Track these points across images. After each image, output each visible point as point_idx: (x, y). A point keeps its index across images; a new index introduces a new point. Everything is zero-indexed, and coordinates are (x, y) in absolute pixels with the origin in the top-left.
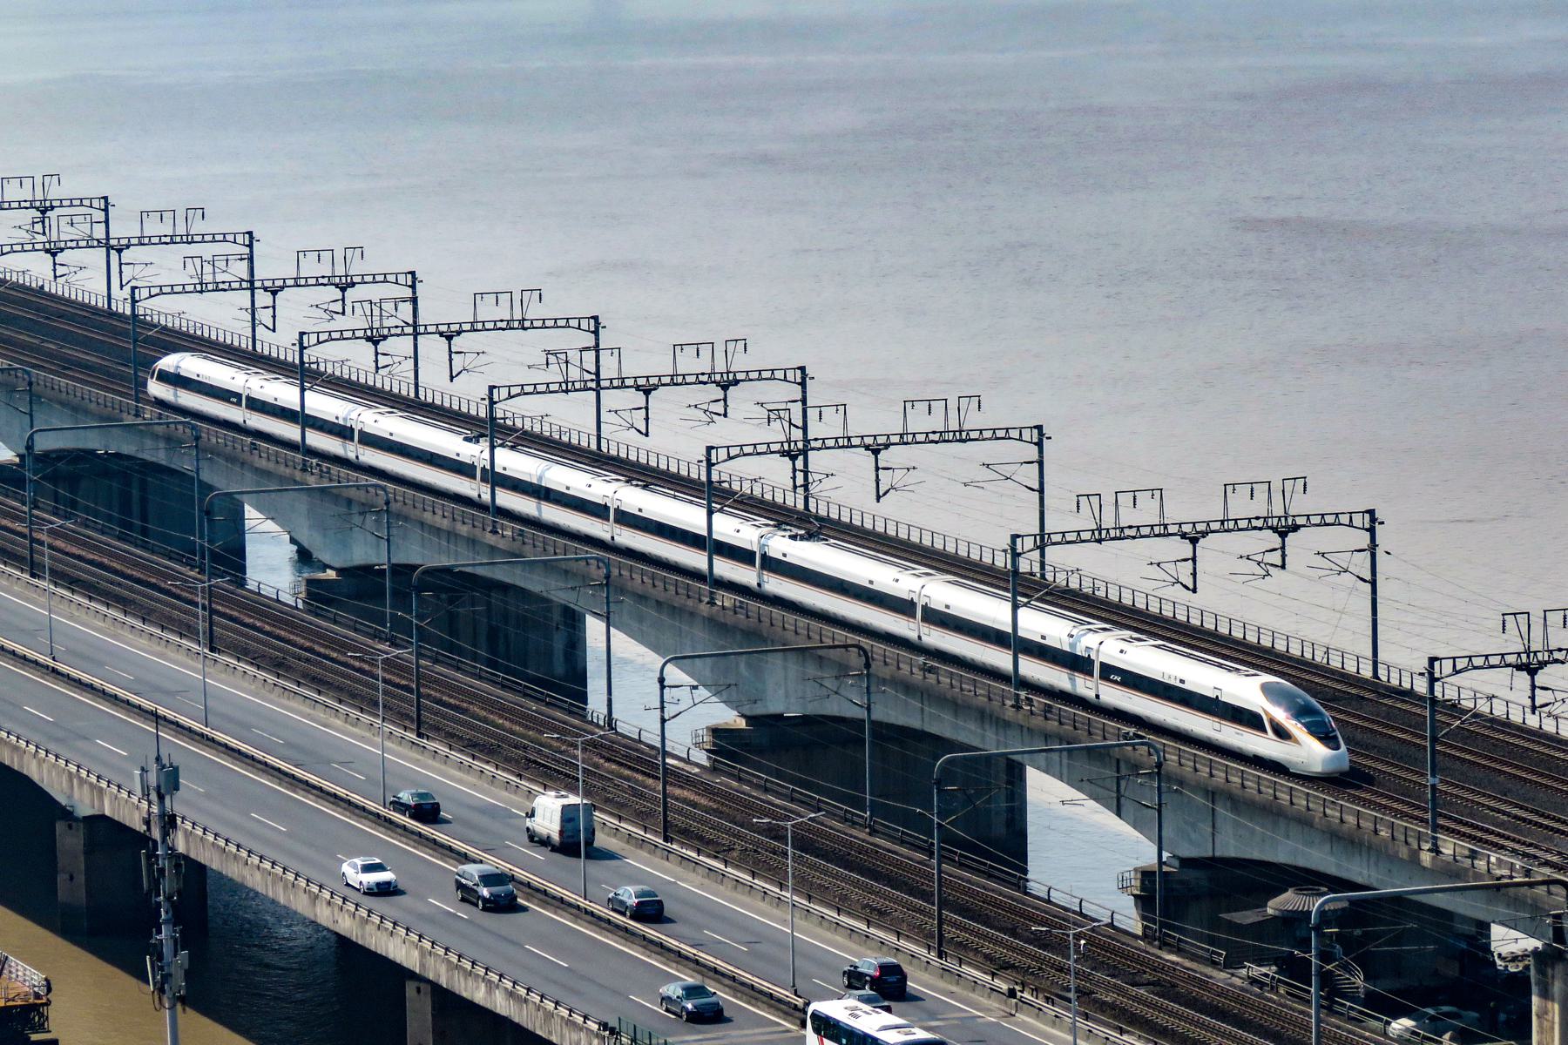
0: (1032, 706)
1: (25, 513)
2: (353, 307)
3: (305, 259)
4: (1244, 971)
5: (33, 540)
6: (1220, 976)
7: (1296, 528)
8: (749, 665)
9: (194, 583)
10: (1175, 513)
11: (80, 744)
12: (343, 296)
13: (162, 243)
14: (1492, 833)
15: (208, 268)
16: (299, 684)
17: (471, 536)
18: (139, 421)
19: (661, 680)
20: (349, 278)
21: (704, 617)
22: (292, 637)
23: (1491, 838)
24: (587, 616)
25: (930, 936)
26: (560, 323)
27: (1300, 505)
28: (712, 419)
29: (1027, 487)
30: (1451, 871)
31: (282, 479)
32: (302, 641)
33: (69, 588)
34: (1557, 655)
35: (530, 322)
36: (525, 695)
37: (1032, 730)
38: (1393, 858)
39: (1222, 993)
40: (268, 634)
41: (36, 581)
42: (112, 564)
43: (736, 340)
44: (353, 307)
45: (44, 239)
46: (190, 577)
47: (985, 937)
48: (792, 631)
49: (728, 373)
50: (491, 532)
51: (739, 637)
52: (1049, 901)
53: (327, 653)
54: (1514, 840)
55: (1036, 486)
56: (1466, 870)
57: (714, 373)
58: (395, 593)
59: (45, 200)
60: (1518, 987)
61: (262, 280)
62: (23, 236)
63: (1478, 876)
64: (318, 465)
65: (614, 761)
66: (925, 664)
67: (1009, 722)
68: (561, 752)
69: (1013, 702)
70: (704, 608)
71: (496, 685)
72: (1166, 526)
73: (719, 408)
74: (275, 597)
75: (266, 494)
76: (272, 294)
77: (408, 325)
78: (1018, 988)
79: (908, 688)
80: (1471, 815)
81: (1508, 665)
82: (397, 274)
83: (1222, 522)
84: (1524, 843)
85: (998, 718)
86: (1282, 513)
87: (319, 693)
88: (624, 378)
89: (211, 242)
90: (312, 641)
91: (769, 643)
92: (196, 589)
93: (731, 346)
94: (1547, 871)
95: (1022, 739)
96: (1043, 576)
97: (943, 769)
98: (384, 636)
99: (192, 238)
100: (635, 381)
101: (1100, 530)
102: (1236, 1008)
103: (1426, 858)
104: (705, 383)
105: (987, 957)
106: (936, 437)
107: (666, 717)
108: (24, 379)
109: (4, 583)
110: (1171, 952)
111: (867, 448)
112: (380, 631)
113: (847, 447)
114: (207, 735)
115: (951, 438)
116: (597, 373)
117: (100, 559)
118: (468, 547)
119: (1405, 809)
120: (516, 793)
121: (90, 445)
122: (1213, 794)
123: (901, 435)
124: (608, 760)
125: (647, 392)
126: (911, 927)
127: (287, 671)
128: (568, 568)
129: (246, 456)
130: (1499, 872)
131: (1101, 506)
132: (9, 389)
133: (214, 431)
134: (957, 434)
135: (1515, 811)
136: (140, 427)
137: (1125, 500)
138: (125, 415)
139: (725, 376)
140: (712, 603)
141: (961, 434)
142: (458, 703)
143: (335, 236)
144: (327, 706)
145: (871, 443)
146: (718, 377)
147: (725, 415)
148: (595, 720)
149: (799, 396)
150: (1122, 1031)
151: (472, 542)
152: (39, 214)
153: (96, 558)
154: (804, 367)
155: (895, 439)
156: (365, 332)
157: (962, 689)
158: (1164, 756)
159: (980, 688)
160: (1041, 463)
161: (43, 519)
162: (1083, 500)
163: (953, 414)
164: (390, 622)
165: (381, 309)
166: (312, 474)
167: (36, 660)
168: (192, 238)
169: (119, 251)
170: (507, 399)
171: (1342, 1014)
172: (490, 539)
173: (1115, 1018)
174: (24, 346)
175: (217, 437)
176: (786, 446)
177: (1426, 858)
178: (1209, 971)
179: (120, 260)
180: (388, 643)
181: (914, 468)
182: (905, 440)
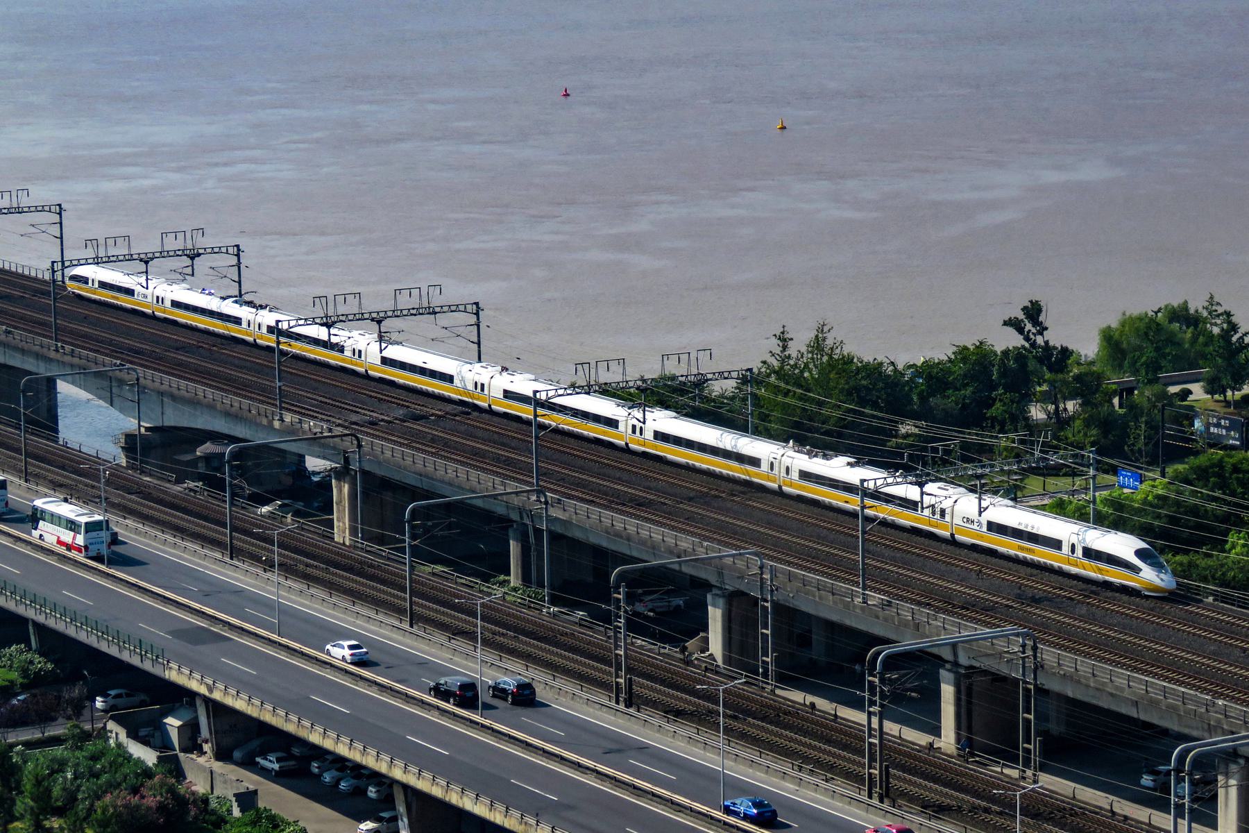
4: (186, 485)
6: (178, 488)
7: (199, 255)
9: (717, 685)
14: (310, 410)
23: (312, 413)
25: (21, 471)
27: (202, 242)
30: (290, 430)
34: (341, 318)
38: (259, 425)
39: (175, 496)
47: (49, 471)
52: (80, 451)
54: (321, 414)
55: (59, 236)
56: (298, 430)
60: (325, 487)
63: (304, 432)
72: (132, 255)
74: (1148, 821)
78: (69, 497)
80: (298, 402)
81: (316, 324)
83: (161, 253)
84: (327, 415)
86: (427, 305)
94: (340, 429)
96: (63, 282)
97: (25, 384)
101: (97, 258)
102: (184, 504)
103: (277, 424)
105: (51, 481)
106: (414, 312)
110: (146, 476)
119: (264, 399)
120: (659, 731)
122: (162, 394)
126: (10, 467)
130: (315, 430)
135: (320, 399)
137: (111, 242)
150: (125, 518)
155: (390, 314)
157: (27, 342)
160: (61, 223)
161: (276, 526)
162: (317, 300)
163: (14, 198)
171: (712, 670)
173: (120, 510)
177: (277, 424)
178: (168, 485)
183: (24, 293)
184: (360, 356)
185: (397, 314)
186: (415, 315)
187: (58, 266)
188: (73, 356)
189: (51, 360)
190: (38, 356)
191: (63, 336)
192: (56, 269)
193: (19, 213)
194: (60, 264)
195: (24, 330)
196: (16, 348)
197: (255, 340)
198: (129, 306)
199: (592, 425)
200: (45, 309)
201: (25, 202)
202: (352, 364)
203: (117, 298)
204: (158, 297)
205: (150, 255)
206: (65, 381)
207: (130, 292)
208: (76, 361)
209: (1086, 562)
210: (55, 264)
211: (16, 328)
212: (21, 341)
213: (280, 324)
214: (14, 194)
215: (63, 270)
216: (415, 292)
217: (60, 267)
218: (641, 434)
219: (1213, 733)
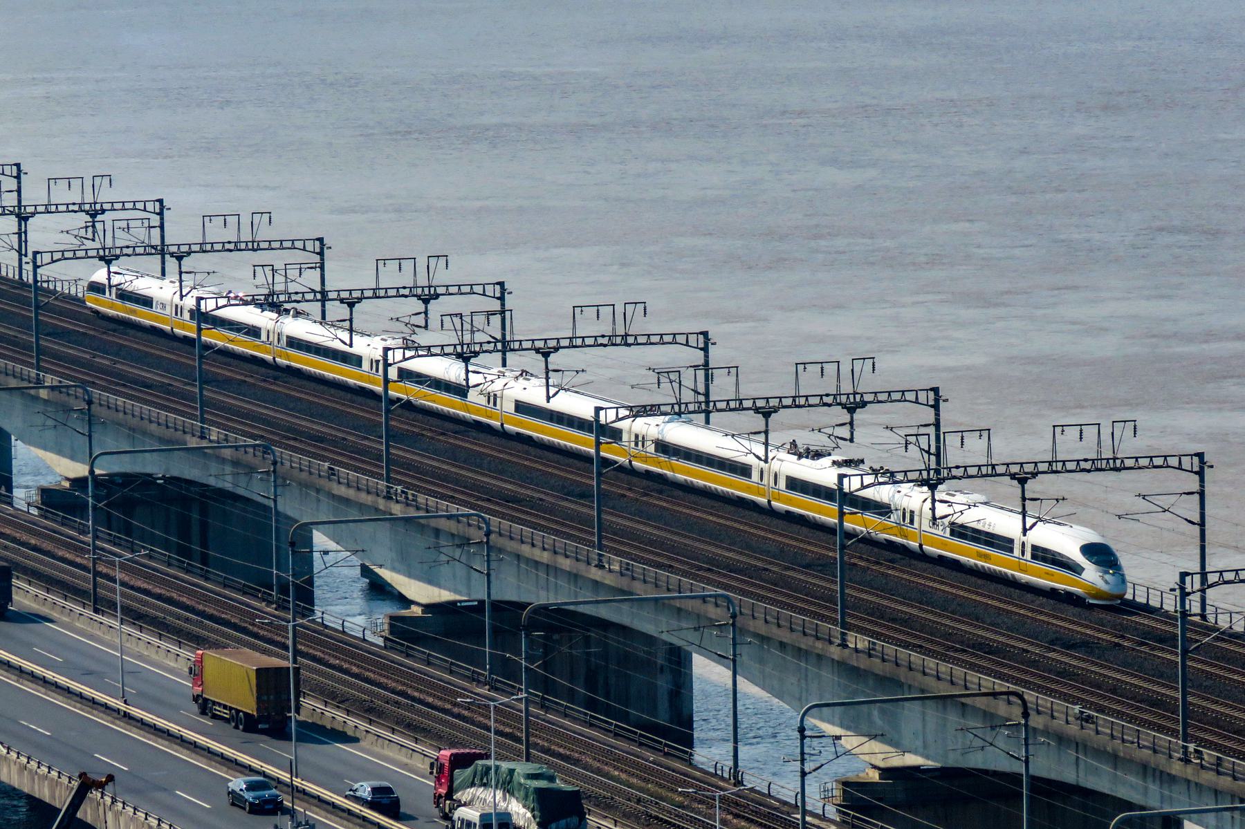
0: (1202, 759)
1: (798, 820)
2: (442, 320)
3: (1063, 437)
5: (97, 574)
8: (883, 712)
9: (712, 791)
10: (748, 390)
11: (160, 795)
12: (426, 308)
13: (69, 212)
15: (279, 279)
16: (393, 731)
17: (575, 571)
18: (204, 444)
19: (802, 730)
20: (432, 289)
21: (833, 659)
22: (383, 680)
24: (694, 655)
26: (666, 339)
28: (414, 331)
29: (1186, 520)
31: (361, 507)
32: (394, 684)
33: (134, 624)
35: (633, 337)
36: (641, 745)
37: (1201, 785)
40: (356, 676)
41: (98, 617)
42: (181, 599)
43: (864, 359)
44: (442, 320)
45: (97, 245)
46: (267, 613)
48: (799, 631)
49: (855, 394)
50: (596, 566)
51: (871, 682)
53: (422, 697)
55: (1197, 519)
57: (840, 394)
58: (496, 631)
59: (95, 203)
61: (339, 291)
62: (70, 241)
64: (403, 492)
65: (743, 817)
66: (1082, 713)
67: (1174, 776)
68: (683, 807)
69: (597, 562)
70: (835, 652)
71: (609, 734)
72: (993, 466)
73: (420, 320)
75: (343, 526)
76: (348, 306)
77: (497, 341)
79: (1062, 740)
82: (145, 202)
83: (1050, 463)
85: (1162, 772)
87: (416, 740)
88: (741, 400)
89: (279, 249)
90: (404, 684)
91: (906, 688)
92: (488, 707)
93: (97, 180)
95: (1189, 795)
96: (1203, 617)
98: (482, 679)
99: (258, 244)
100: (754, 402)
104: (829, 405)
106: (1087, 465)
107: (807, 770)
108: (480, 528)
109: (64, 619)
111: (537, 351)
112: (479, 674)
113: (991, 476)
114: (297, 787)
115: (1104, 467)
116: (707, 394)
117: (168, 594)
118: (833, 672)
121: (148, 470)
123: (1050, 462)
124: (737, 816)
125: (767, 415)
127: (379, 717)
128: (683, 607)
129: (324, 483)
131: (105, 231)
132: (457, 542)
133: (189, 423)
134: (1111, 461)
136: (206, 451)
138: (188, 437)
139: (851, 397)
140: (844, 645)
141: (1114, 462)
142: (568, 753)
143: (246, 202)
144: (425, 755)
145: (542, 346)
146: (844, 399)
147: (851, 440)
148: (719, 772)
149: (15, 188)
151: (574, 577)
152: (88, 218)
153: (163, 592)
154: (19, 164)
156: (455, 347)
157: (1123, 741)
158: (740, 611)
159: (1144, 740)
160: (1202, 494)
163: (89, 190)
164: (490, 664)
165: (286, 276)
166: (397, 502)
167: (106, 704)
168: (258, 244)
169: (180, 258)
170: (50, 263)
172: (595, 574)
174: (74, 361)
175: (291, 461)
176: (459, 349)
179: (180, 267)
180: (487, 687)
181: (583, 371)
182: (1054, 469)
183: (1123, 637)
184: (912, 522)
185: (1055, 467)
186: (1089, 471)
187: (1194, 583)
188: (1219, 773)
189: (1172, 779)
190: (1145, 770)
191: (399, 473)
192: (1189, 589)
193: (253, 250)
194: (1197, 578)
195: (1119, 715)
196: (1099, 753)
197: (769, 502)
198: (148, 322)
199: (445, 396)
200: (1163, 673)
201: (1129, 446)
202: (370, 383)
203: (133, 312)
204: (637, 436)
205: (1029, 468)
206: (1199, 823)
207: (744, 470)
208: (1225, 782)
209: (119, 303)
210: (1188, 579)
211: (1101, 710)
212: (1112, 737)
213: (203, 302)
214: (88, 183)
215: (1203, 591)
216: (830, 369)
217: (1197, 586)
218: (776, 484)
219: (1219, 798)
